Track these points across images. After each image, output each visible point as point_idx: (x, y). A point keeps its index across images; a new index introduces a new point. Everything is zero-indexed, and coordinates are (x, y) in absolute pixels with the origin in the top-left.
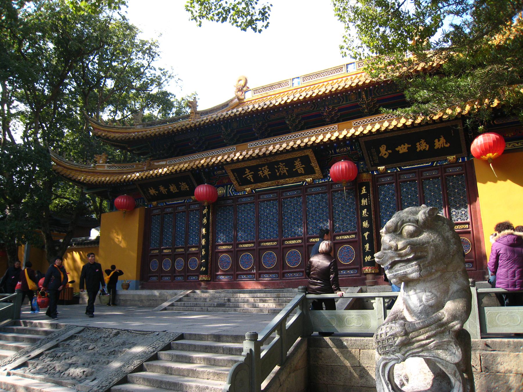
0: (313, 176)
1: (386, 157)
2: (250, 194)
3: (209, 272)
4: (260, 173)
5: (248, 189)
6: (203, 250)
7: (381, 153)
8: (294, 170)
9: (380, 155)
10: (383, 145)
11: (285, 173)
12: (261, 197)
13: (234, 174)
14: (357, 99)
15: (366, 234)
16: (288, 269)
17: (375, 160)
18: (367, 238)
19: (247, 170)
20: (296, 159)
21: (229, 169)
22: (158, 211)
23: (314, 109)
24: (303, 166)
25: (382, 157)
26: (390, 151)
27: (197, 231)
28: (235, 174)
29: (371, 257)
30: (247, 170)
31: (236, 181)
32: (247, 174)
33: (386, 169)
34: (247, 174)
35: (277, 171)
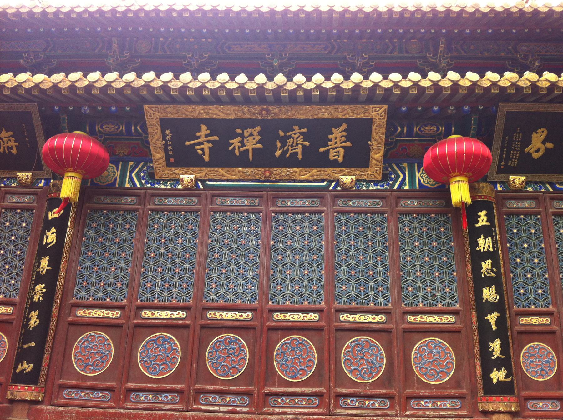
0: (358, 172)
1: (536, 156)
2: (189, 192)
3: (42, 378)
4: (236, 142)
5: (187, 178)
6: (34, 315)
7: (530, 146)
8: (322, 150)
9: (527, 150)
10: (542, 129)
11: (297, 153)
12: (218, 200)
13: (163, 132)
14: (422, 52)
15: (492, 318)
16: (279, 386)
17: (511, 159)
18: (494, 328)
19: (204, 127)
20: (337, 123)
21: (158, 115)
22: (526, 204)
23: (330, 52)
24: (348, 144)
25: (529, 154)
26: (549, 145)
27: (19, 264)
28: (168, 132)
29: (505, 372)
30: (204, 127)
31: (163, 153)
32: (199, 137)
33: (527, 183)
34: (199, 137)
35: (279, 144)
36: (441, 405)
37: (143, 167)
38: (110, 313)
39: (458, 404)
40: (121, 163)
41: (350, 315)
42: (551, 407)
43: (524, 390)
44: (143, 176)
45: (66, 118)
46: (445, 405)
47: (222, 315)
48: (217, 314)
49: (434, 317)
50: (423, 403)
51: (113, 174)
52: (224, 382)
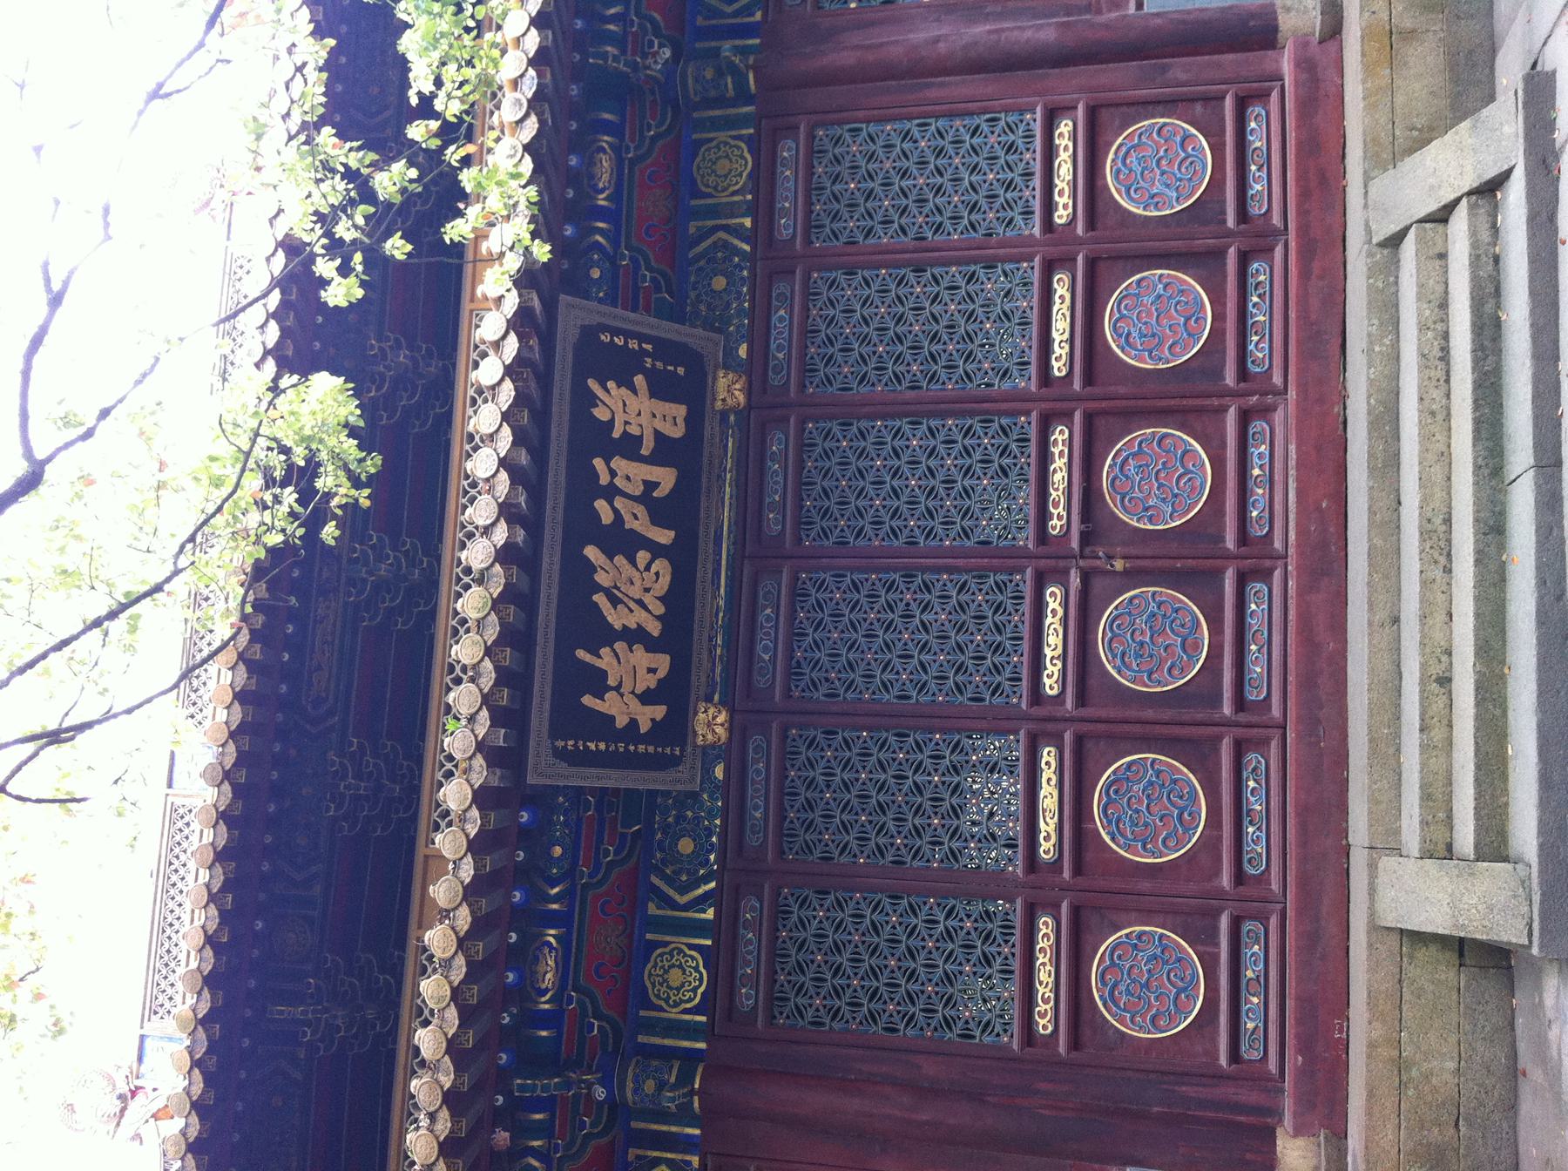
36: (1261, 467)
37: (664, 877)
38: (1041, 945)
39: (1259, 429)
40: (634, 1124)
41: (1046, 668)
42: (1256, 947)
43: (1224, 221)
44: (688, 873)
45: (519, 1081)
46: (1261, 456)
47: (1052, 658)
48: (1042, 1007)
49: (1055, 471)
50: (1250, 1025)
51: (678, 954)
52: (1218, 317)
